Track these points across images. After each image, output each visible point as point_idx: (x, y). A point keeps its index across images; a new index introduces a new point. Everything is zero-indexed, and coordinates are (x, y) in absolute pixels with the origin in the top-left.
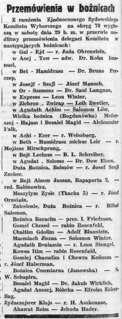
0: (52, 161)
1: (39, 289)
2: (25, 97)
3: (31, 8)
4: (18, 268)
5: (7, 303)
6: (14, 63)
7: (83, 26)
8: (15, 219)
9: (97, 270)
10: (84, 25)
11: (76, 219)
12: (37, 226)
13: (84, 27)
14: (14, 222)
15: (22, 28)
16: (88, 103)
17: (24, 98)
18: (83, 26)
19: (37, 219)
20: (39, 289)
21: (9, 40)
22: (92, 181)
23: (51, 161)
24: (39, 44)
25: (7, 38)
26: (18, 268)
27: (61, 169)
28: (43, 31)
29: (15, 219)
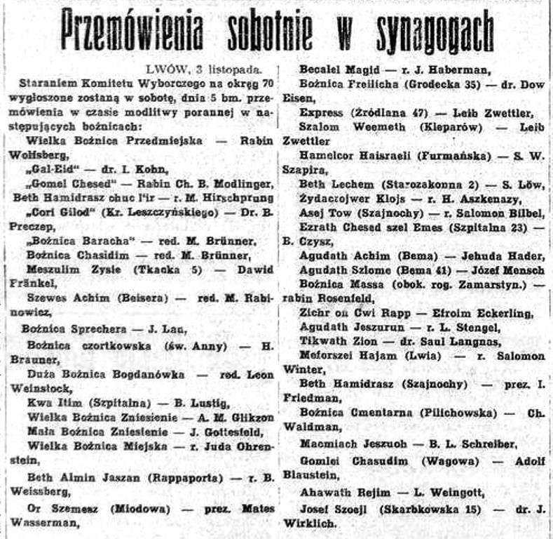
0: (364, 271)
1: (203, 345)
2: (310, 111)
3: (262, 21)
4: (313, 221)
5: (306, 198)
6: (540, 210)
7: (240, 84)
8: (303, 184)
9: (496, 413)
10: (243, 83)
11: (512, 443)
12: (88, 256)
13: (243, 86)
14: (302, 191)
15: (306, 145)
16: (379, 313)
17: (308, 113)
18: (240, 84)
19: (87, 240)
20: (203, 345)
21: (244, 185)
22: (441, 384)
23: (363, 269)
24: (404, 441)
25: (239, 181)
26: (313, 221)
27: (495, 447)
28: (251, 66)
29: (303, 184)
